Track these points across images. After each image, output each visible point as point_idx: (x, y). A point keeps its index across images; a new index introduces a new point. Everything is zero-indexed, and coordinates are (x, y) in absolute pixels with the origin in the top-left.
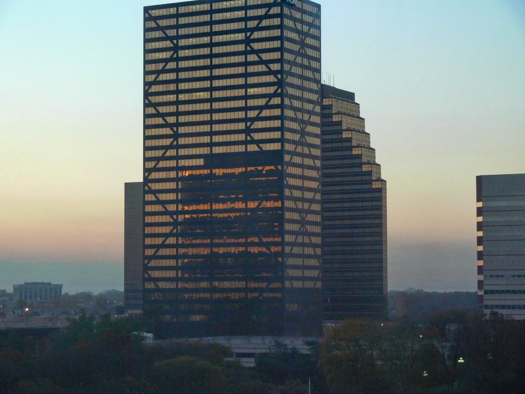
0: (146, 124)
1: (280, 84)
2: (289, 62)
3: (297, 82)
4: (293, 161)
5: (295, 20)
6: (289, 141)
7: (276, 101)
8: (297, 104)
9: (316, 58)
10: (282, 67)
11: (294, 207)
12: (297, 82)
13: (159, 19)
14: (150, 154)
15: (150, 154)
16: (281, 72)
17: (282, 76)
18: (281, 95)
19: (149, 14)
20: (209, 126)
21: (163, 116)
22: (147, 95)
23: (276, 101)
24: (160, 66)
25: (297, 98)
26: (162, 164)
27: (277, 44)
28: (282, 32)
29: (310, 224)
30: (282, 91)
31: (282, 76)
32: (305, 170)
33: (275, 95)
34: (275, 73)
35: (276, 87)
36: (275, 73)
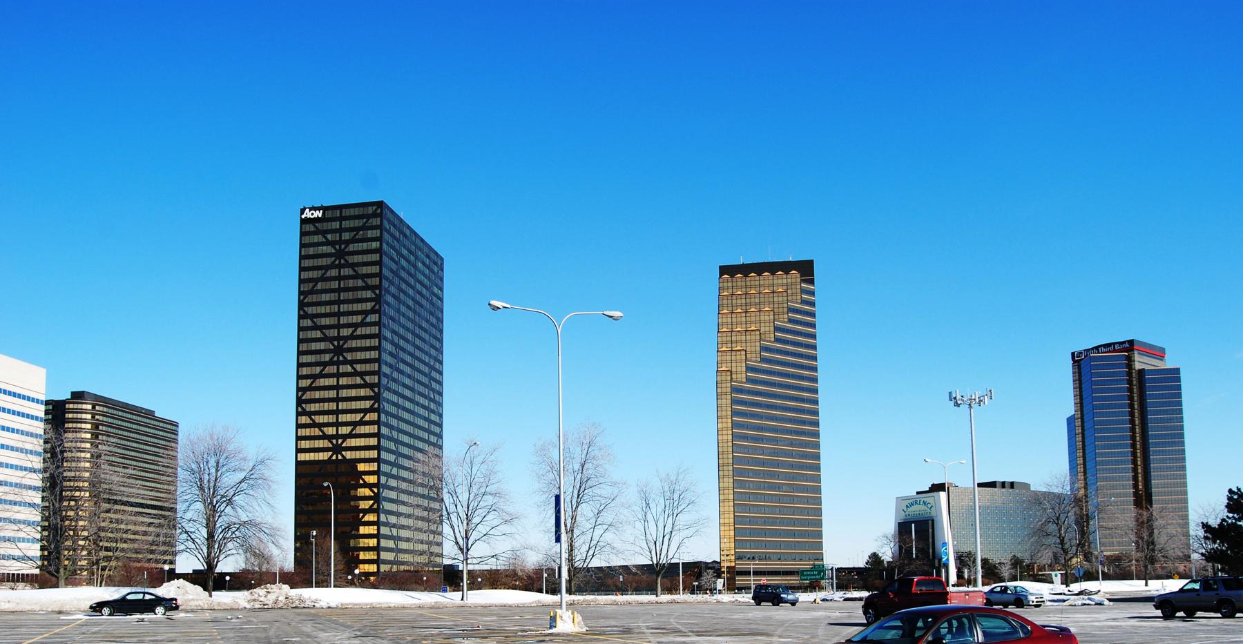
0: (302, 277)
1: (376, 398)
2: (386, 474)
3: (393, 398)
4: (389, 484)
5: (391, 427)
6: (385, 562)
7: (373, 416)
8: (393, 422)
9: (410, 445)
10: (379, 479)
11: (388, 516)
12: (393, 398)
13: (315, 415)
14: (306, 275)
15: (306, 275)
16: (377, 485)
17: (379, 490)
18: (377, 410)
19: (304, 311)
20: (335, 428)
21: (320, 426)
22: (302, 305)
23: (374, 416)
25: (394, 416)
26: (357, 319)
27: (373, 454)
28: (379, 454)
29: (408, 433)
30: (379, 406)
31: (379, 490)
32: (400, 411)
33: (371, 410)
34: (371, 386)
35: (373, 304)
36: (371, 386)
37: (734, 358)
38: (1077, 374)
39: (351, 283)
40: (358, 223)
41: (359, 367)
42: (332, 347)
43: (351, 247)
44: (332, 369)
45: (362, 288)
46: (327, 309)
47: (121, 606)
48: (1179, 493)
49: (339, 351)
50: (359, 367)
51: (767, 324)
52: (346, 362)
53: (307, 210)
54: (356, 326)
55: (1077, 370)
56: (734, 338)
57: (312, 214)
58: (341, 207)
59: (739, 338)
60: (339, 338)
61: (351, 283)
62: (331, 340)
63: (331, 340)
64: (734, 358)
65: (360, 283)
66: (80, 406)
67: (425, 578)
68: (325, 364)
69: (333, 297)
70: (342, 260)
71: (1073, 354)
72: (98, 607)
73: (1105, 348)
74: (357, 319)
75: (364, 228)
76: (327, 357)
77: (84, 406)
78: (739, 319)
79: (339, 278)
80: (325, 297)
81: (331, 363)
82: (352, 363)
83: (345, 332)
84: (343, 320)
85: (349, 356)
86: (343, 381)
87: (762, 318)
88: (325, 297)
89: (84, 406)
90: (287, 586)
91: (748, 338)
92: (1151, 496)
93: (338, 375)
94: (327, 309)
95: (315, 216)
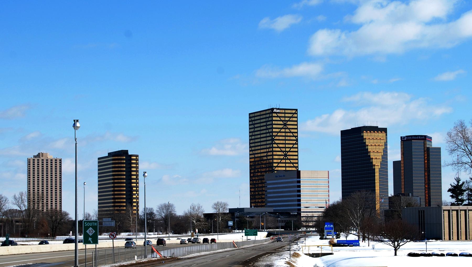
24: (291, 119)
26: (291, 146)
35: (296, 141)
37: (377, 161)
38: (403, 146)
39: (289, 134)
40: (290, 115)
41: (292, 161)
42: (283, 154)
43: (289, 123)
44: (284, 161)
45: (292, 136)
46: (282, 142)
47: (177, 239)
48: (437, 196)
49: (286, 155)
50: (292, 161)
51: (381, 150)
52: (288, 159)
53: (275, 109)
54: (291, 148)
55: (403, 144)
56: (375, 154)
57: (277, 111)
58: (285, 109)
59: (376, 154)
60: (285, 151)
61: (289, 134)
62: (283, 152)
63: (283, 152)
64: (377, 161)
65: (291, 134)
66: (121, 157)
67: (49, 234)
68: (281, 159)
69: (283, 138)
70: (286, 127)
71: (401, 137)
72: (167, 239)
73: (415, 137)
74: (291, 146)
75: (292, 117)
76: (282, 157)
77: (123, 157)
78: (374, 148)
79: (285, 132)
80: (281, 138)
81: (283, 159)
82: (290, 159)
83: (288, 150)
84: (287, 146)
85: (289, 157)
86: (287, 165)
87: (380, 148)
88: (281, 138)
89: (123, 157)
90: (4, 241)
91: (379, 154)
92: (430, 196)
93: (286, 163)
94: (282, 142)
95: (278, 111)
